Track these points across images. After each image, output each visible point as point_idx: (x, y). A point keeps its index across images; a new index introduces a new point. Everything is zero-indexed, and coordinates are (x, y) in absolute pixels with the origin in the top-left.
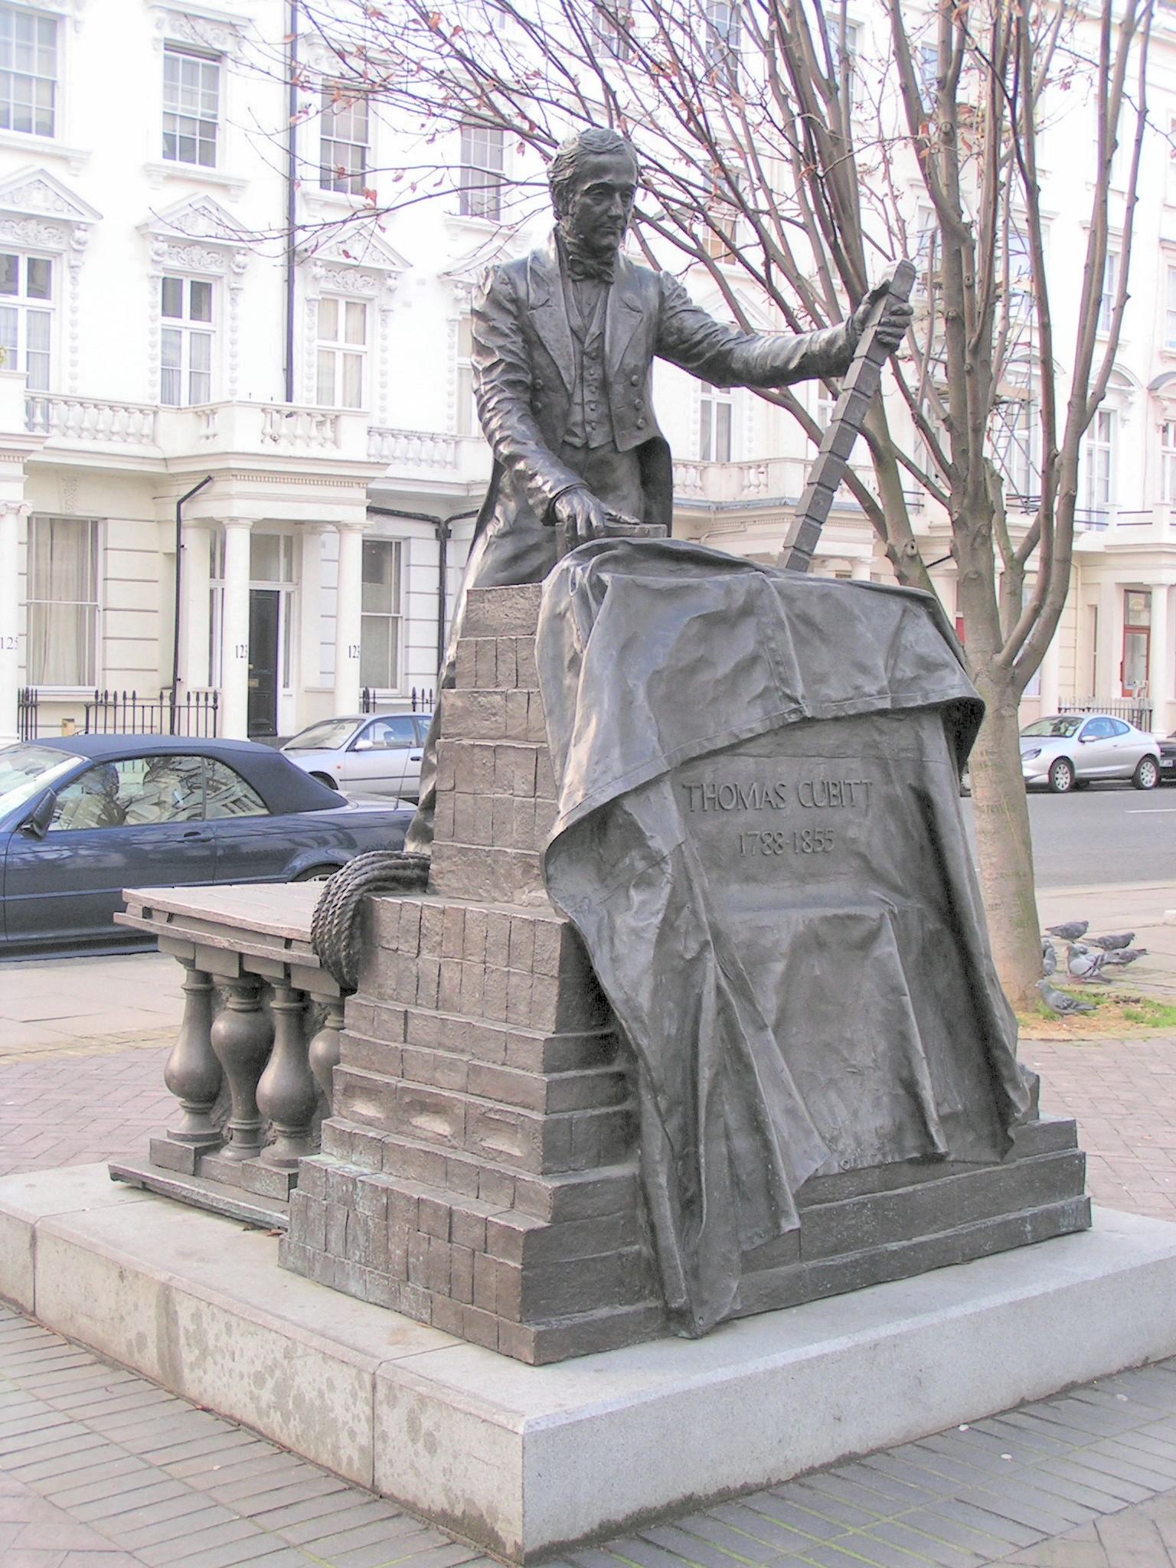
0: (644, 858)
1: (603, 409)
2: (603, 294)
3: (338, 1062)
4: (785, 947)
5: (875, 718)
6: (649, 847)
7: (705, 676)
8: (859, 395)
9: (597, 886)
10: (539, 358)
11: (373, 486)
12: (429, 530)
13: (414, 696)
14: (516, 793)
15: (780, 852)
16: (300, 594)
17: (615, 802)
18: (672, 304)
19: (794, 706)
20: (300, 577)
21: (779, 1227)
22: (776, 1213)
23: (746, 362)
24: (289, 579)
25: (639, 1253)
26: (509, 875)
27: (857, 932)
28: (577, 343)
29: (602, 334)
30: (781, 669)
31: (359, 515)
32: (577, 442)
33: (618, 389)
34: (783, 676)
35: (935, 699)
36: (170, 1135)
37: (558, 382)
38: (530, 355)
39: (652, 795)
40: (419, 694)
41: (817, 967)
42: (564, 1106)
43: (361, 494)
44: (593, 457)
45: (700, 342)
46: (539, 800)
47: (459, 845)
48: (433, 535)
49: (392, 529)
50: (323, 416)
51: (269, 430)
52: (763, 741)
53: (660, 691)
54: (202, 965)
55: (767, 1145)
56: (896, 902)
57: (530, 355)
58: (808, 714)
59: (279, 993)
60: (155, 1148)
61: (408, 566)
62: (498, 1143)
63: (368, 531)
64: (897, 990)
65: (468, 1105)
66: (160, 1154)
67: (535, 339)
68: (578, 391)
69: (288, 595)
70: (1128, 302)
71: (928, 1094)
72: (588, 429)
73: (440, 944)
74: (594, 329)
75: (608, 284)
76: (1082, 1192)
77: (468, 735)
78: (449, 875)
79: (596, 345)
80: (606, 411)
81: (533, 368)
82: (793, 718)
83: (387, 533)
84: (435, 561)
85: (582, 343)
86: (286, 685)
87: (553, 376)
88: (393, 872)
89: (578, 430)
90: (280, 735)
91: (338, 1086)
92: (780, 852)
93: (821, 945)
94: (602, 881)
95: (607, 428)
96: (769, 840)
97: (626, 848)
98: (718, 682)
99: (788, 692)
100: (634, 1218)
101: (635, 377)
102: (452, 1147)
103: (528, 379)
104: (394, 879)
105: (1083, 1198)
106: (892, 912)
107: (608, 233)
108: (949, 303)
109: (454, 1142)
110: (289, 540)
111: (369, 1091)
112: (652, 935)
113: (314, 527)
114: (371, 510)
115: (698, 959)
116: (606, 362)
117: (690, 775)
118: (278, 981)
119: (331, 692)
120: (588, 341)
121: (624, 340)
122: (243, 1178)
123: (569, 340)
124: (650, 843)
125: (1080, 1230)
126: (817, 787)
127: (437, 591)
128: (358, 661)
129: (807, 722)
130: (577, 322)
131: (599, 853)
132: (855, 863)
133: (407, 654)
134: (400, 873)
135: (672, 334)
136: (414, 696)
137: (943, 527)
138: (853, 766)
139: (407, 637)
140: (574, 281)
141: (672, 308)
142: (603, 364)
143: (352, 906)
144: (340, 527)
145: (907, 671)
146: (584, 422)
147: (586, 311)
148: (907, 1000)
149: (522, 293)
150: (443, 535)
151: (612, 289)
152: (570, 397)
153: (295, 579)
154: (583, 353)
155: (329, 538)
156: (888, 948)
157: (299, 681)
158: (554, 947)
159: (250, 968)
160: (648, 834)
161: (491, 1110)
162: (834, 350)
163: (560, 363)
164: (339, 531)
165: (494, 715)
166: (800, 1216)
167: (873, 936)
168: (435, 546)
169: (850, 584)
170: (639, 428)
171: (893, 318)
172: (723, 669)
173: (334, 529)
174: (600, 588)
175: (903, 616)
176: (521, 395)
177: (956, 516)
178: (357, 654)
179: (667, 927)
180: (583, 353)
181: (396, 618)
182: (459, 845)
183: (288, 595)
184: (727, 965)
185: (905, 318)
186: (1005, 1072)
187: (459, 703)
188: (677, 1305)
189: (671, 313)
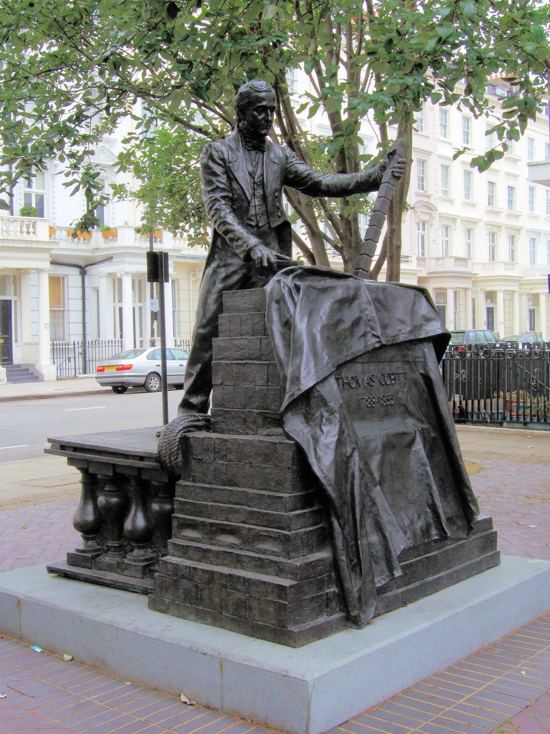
0: (327, 411)
1: (264, 209)
2: (261, 156)
3: (173, 513)
4: (380, 448)
5: (406, 344)
6: (329, 406)
7: (342, 327)
8: (386, 200)
9: (305, 425)
10: (235, 186)
11: (52, 252)
12: (77, 271)
13: (74, 345)
14: (256, 384)
15: (374, 405)
16: (21, 301)
17: (314, 386)
18: (291, 160)
19: (377, 340)
20: (20, 293)
21: (393, 575)
22: (391, 569)
23: (328, 186)
24: (15, 294)
25: (335, 592)
26: (254, 422)
27: (408, 438)
28: (252, 178)
29: (263, 174)
30: (371, 323)
31: (46, 265)
32: (253, 224)
33: (270, 199)
34: (372, 326)
35: (431, 334)
36: (78, 550)
37: (243, 197)
38: (230, 184)
39: (326, 383)
40: (76, 343)
41: (392, 456)
42: (298, 527)
43: (47, 256)
44: (261, 230)
45: (306, 177)
46: (270, 387)
47: (226, 409)
48: (79, 273)
49: (61, 271)
50: (29, 221)
51: (5, 228)
52: (365, 356)
53: (326, 333)
54: (91, 470)
55: (384, 537)
56: (420, 426)
57: (230, 184)
58: (384, 343)
59: (133, 482)
60: (70, 556)
61: (68, 287)
62: (268, 546)
63: (50, 272)
64: (423, 465)
65: (250, 529)
66: (73, 559)
67: (232, 176)
68: (253, 200)
69: (15, 302)
70: (14, 198)
71: (441, 511)
72: (258, 218)
73: (226, 456)
74: (259, 172)
75: (263, 152)
76: (496, 549)
77: (227, 358)
78: (222, 424)
79: (259, 179)
80: (265, 209)
81: (232, 190)
82: (377, 345)
83: (58, 273)
84: (80, 284)
85: (254, 179)
86: (16, 341)
87: (241, 193)
88: (193, 423)
89: (253, 218)
90: (14, 364)
91: (175, 524)
92: (374, 405)
93: (394, 447)
94: (307, 423)
95: (265, 217)
96: (369, 400)
97: (318, 407)
98: (346, 330)
99: (375, 333)
100: (331, 576)
101: (277, 194)
102: (240, 549)
103: (231, 195)
104: (195, 426)
105: (498, 551)
106: (418, 430)
107: (265, 128)
108: (338, 165)
109: (241, 546)
110: (14, 277)
111: (193, 526)
112: (333, 446)
113: (67, 275)
114: (53, 263)
115: (351, 456)
116: (265, 187)
117: (347, 373)
118: (135, 477)
119: (37, 344)
120: (256, 177)
121: (271, 178)
122: (120, 568)
123: (248, 177)
124: (329, 404)
125: (497, 565)
126: (386, 376)
127: (81, 298)
128: (49, 330)
129: (383, 346)
130: (251, 169)
131: (306, 410)
132: (403, 408)
133: (69, 326)
134: (197, 423)
135: (292, 174)
136: (74, 345)
137: (341, 263)
138: (398, 365)
139: (69, 318)
140: (248, 150)
141: (291, 162)
142: (263, 188)
143: (178, 440)
144: (39, 271)
145: (418, 321)
146: (256, 215)
147: (254, 164)
148: (429, 468)
149: (226, 157)
150: (83, 273)
151: (265, 153)
152: (249, 202)
153: (18, 294)
154: (254, 183)
155: (32, 279)
156: (419, 446)
157: (22, 339)
158: (288, 454)
159: (118, 471)
160: (328, 400)
161: (261, 531)
162: (371, 180)
163: (244, 187)
164: (38, 273)
165: (242, 349)
166: (403, 568)
167: (413, 441)
168: (79, 278)
169: (397, 285)
170: (279, 217)
171: (399, 165)
172: (347, 324)
173: (35, 272)
174: (298, 288)
175: (415, 297)
176: (228, 203)
177: (347, 258)
178: (48, 327)
179: (340, 443)
180: (254, 183)
181: (63, 311)
182: (226, 409)
183: (15, 302)
184: (361, 456)
185: (404, 165)
186: (469, 498)
187: (222, 344)
188: (354, 614)
189: (290, 165)
